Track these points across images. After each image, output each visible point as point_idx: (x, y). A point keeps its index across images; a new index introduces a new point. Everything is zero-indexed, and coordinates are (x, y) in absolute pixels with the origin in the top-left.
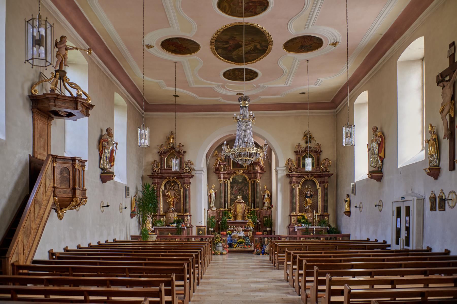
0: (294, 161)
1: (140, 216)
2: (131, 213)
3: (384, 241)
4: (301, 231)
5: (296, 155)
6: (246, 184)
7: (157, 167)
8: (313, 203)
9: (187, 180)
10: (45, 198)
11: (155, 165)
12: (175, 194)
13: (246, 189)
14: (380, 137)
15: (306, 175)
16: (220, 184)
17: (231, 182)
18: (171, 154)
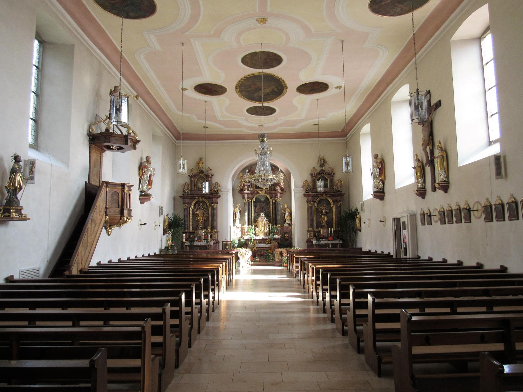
2: (164, 230)
3: (388, 252)
5: (312, 177)
7: (188, 189)
10: (99, 217)
11: (186, 187)
12: (203, 213)
14: (381, 163)
15: (321, 195)
16: (245, 203)
17: (254, 202)
18: (201, 177)
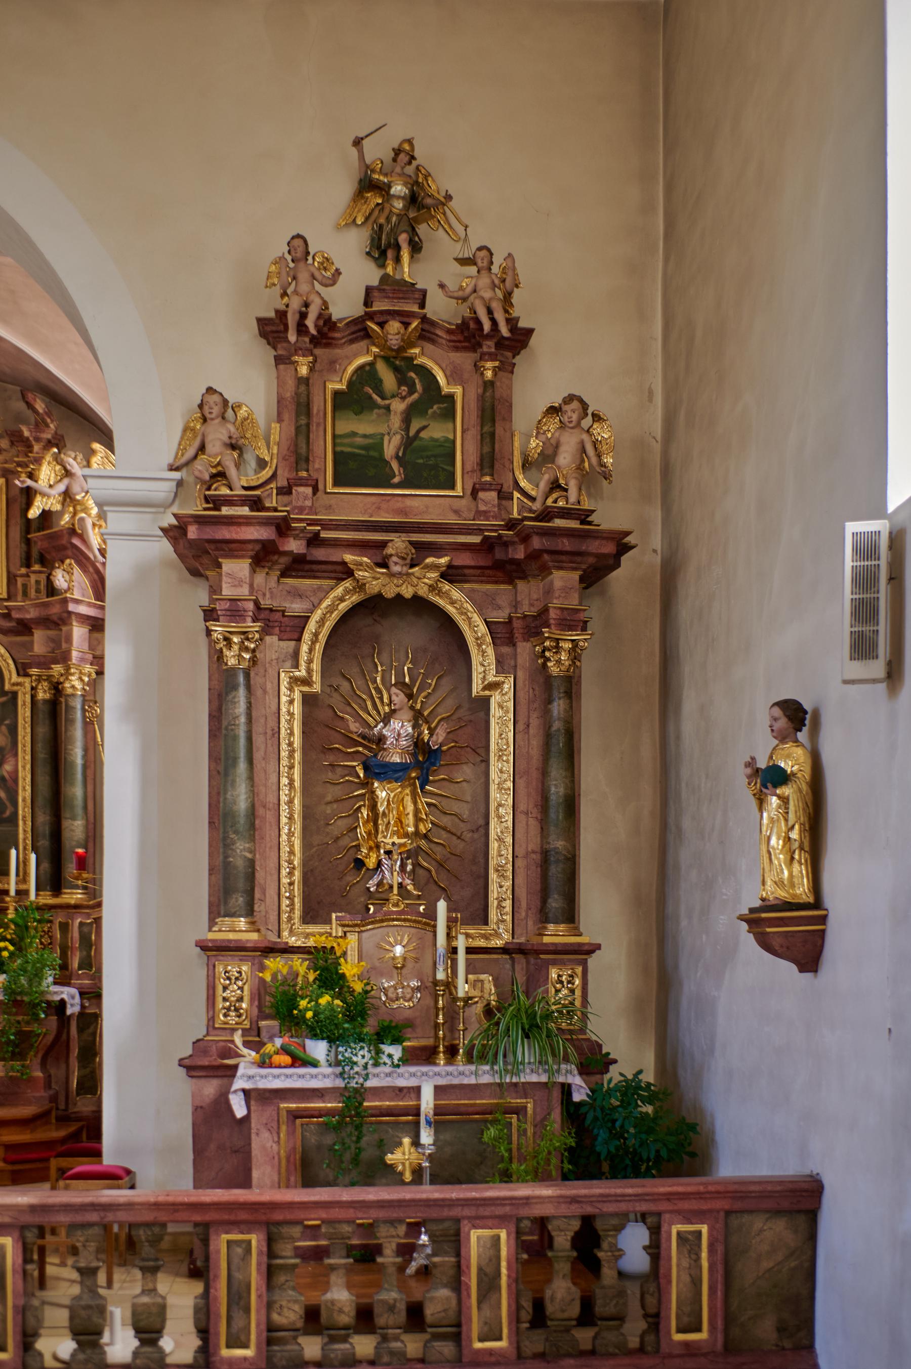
0: (261, 420)
4: (295, 1115)
8: (440, 838)
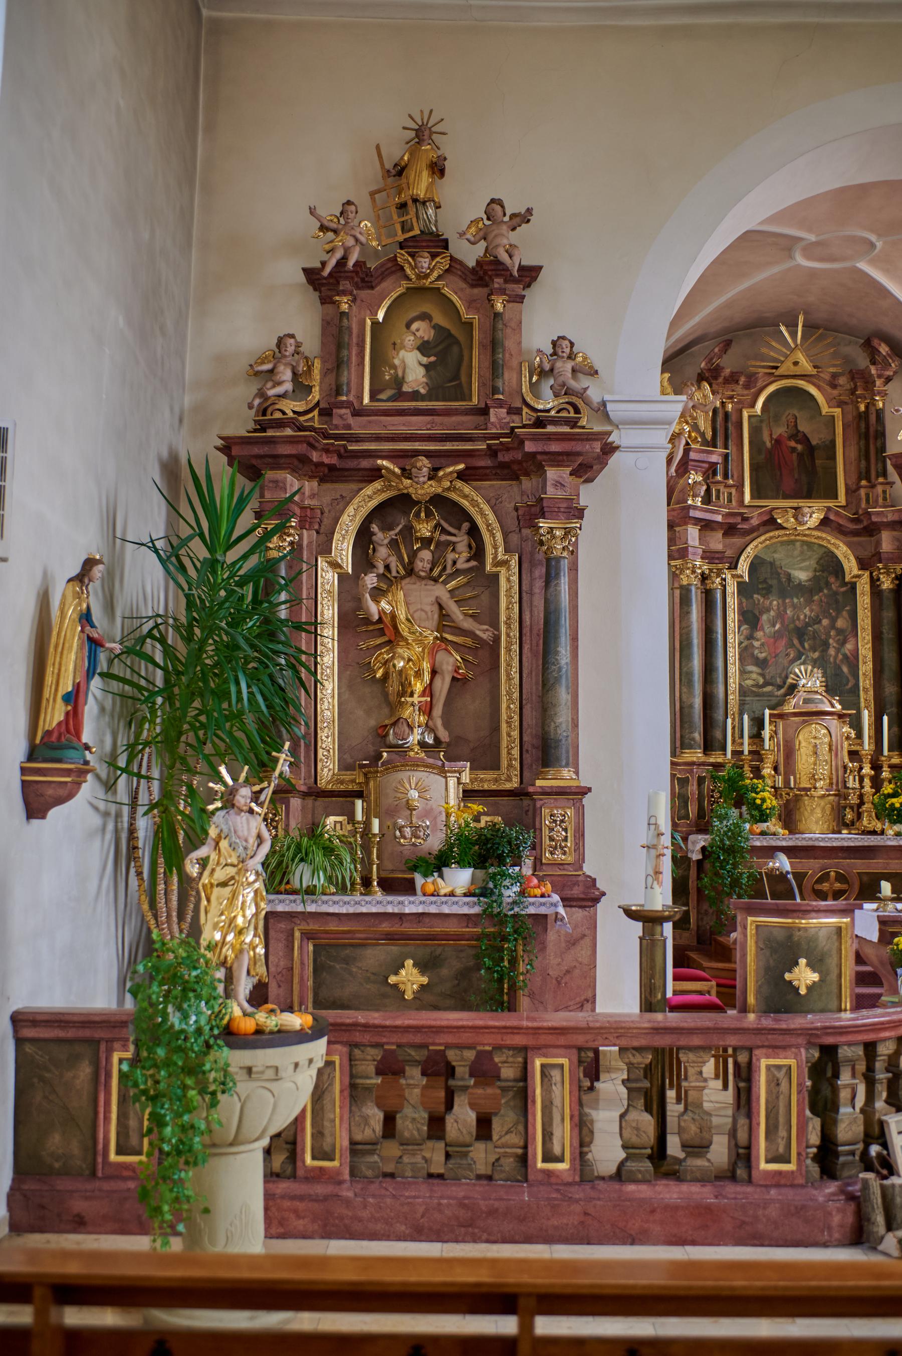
1: (134, 799)
2: (32, 754)
6: (840, 598)
9: (559, 484)
13: (840, 632)
17: (743, 589)
